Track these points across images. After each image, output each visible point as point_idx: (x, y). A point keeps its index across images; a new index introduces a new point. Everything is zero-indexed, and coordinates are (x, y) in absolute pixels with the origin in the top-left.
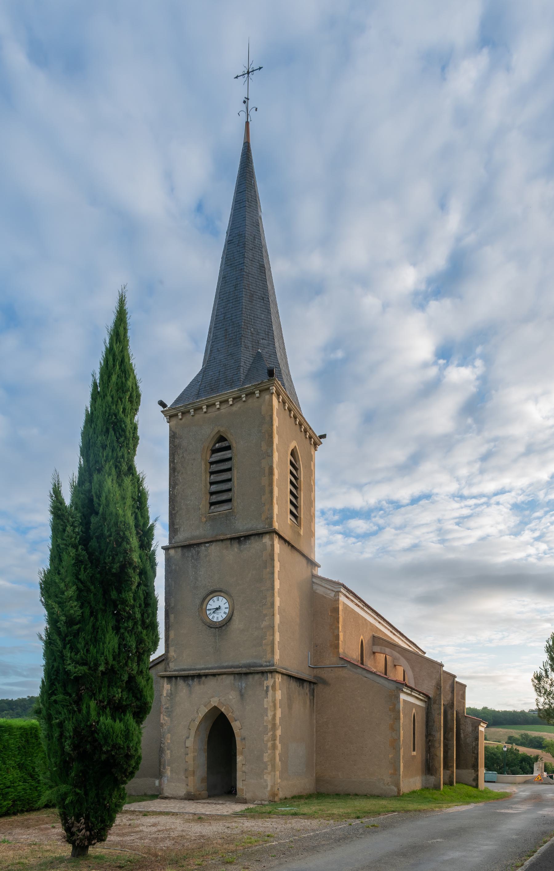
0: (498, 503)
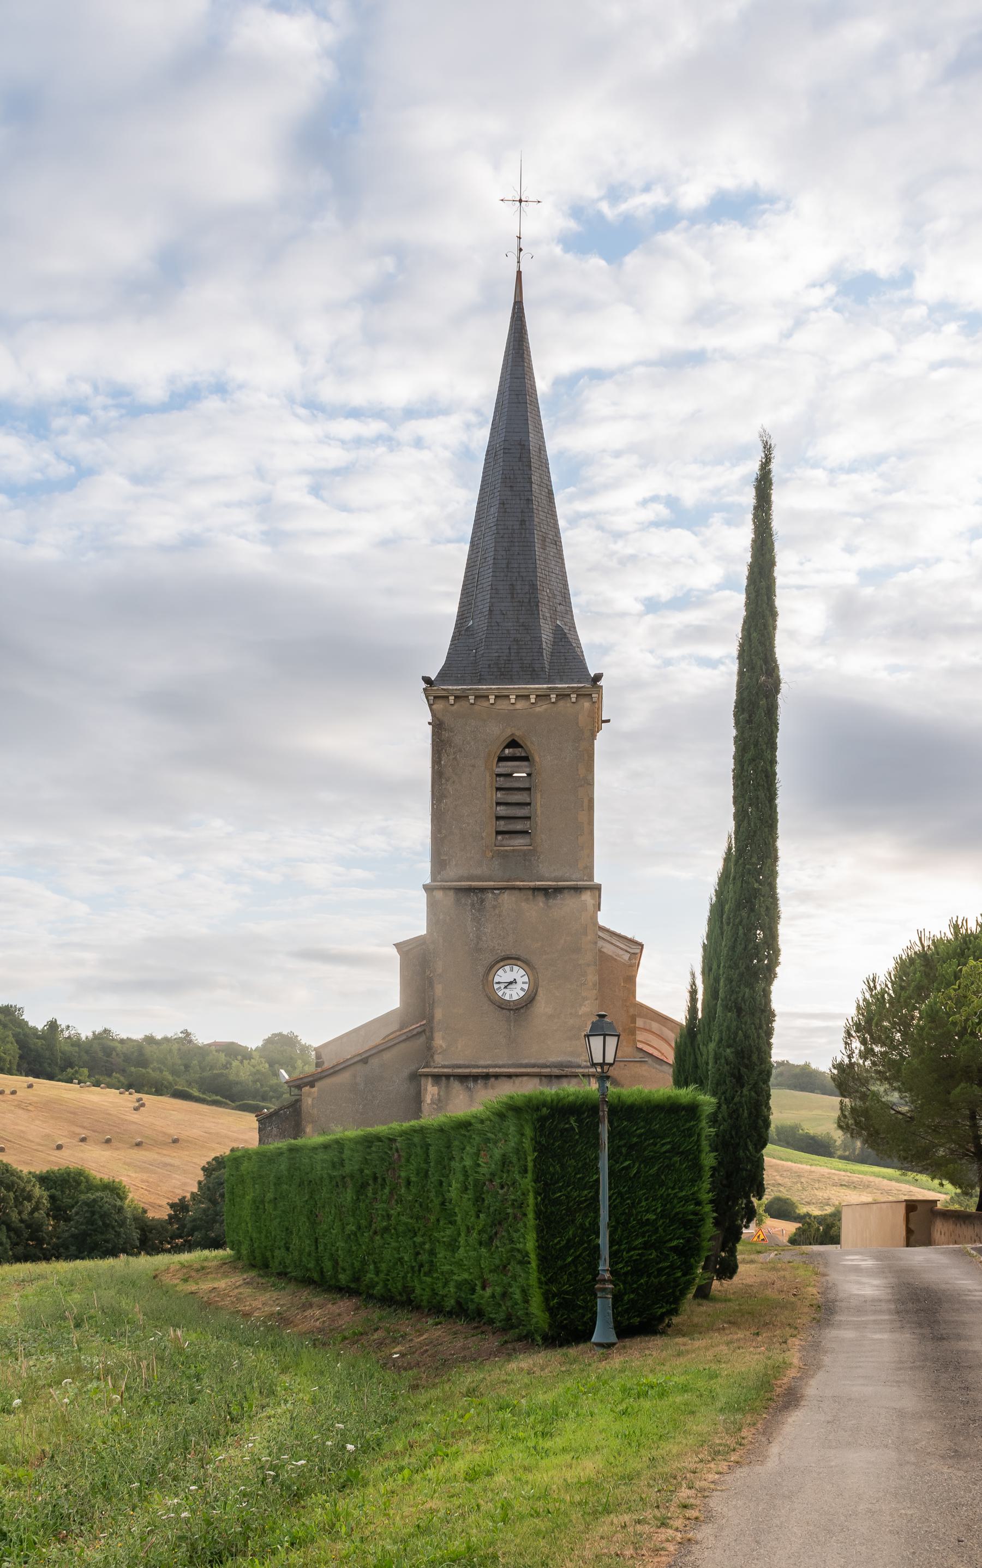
0: (419, 443)
